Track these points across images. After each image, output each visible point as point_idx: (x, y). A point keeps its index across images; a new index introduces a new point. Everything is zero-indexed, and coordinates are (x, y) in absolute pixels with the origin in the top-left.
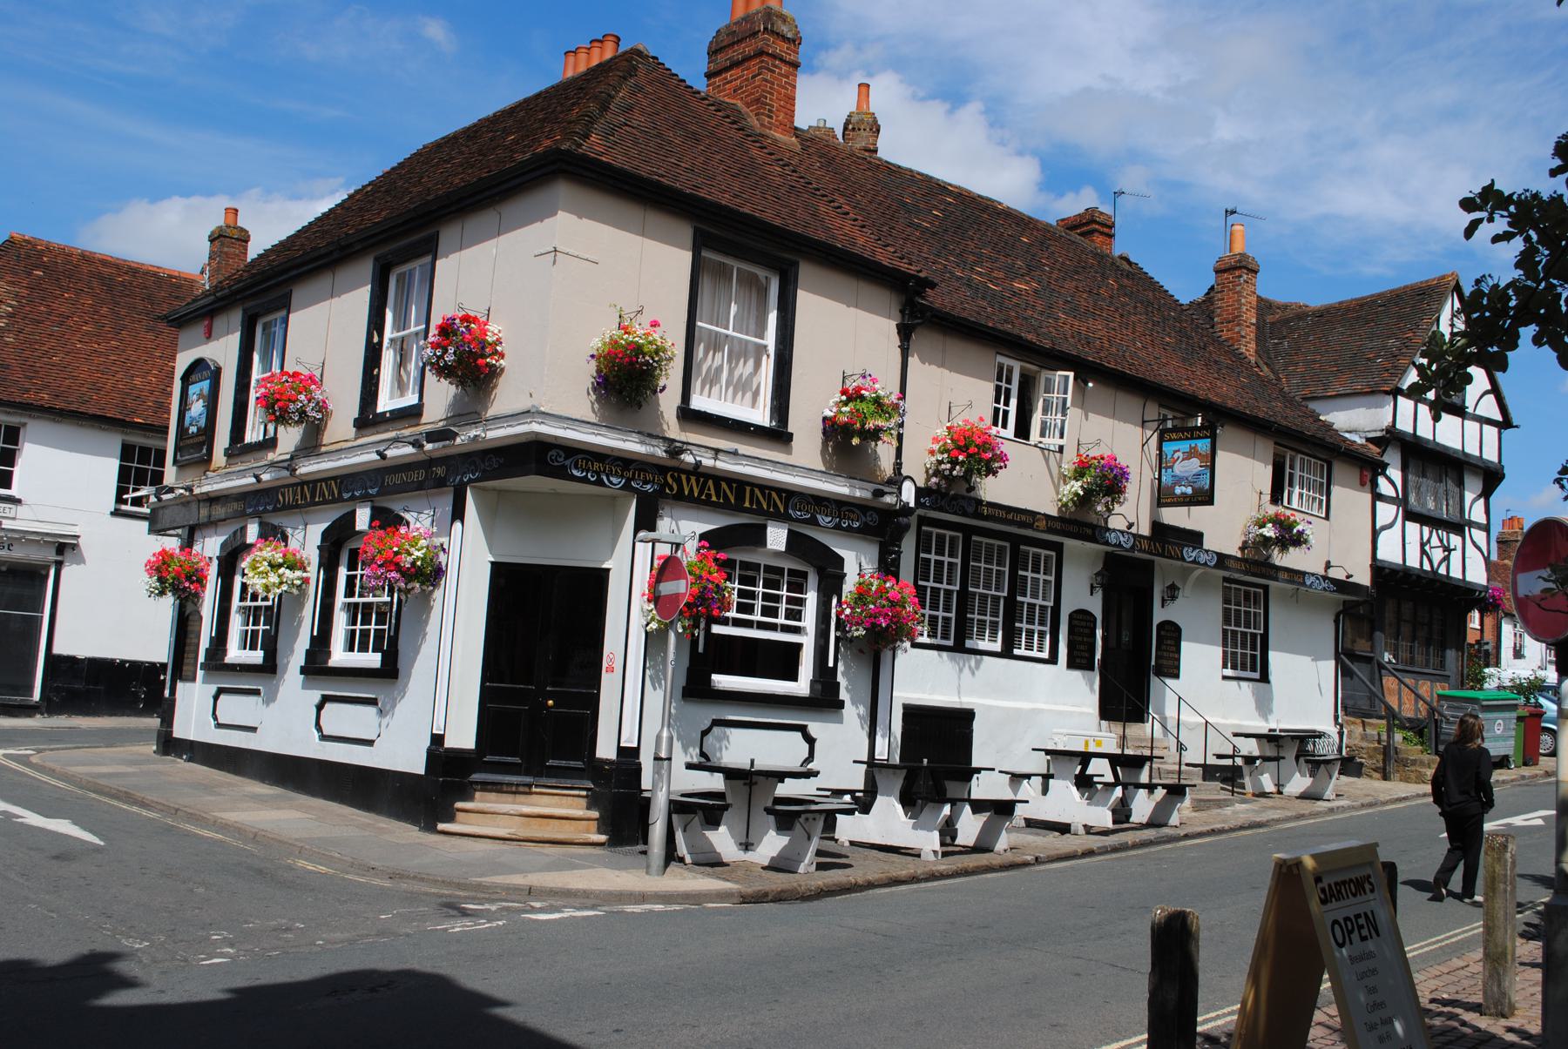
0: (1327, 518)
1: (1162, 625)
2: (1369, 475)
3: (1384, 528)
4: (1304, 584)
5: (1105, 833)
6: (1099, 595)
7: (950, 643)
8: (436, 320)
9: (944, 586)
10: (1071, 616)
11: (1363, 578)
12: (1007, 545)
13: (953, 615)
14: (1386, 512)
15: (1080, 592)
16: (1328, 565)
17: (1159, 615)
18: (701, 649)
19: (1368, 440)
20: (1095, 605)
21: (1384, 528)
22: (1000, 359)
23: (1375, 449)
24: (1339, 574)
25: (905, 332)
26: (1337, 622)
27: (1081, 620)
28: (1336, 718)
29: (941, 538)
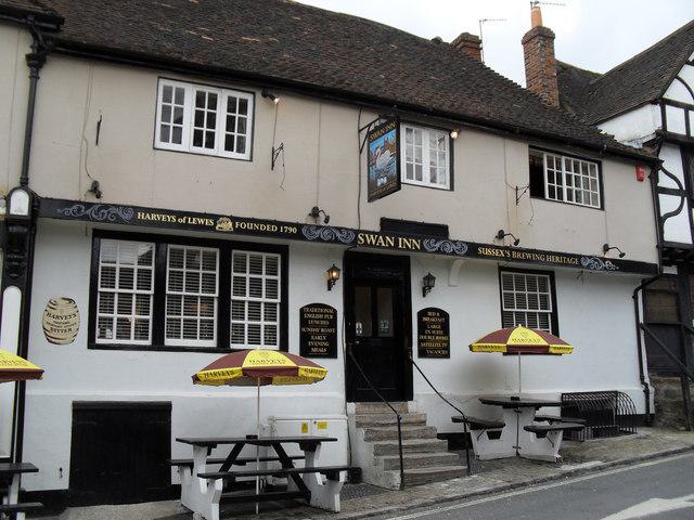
0: (602, 208)
1: (422, 314)
2: (646, 173)
3: (669, 215)
4: (580, 265)
5: (557, 420)
6: (339, 287)
7: (148, 343)
8: (556, 268)
9: (263, 299)
10: (302, 311)
11: (650, 256)
12: (217, 251)
13: (150, 317)
14: (669, 203)
15: (313, 286)
16: (606, 248)
17: (418, 304)
18: (641, 320)
19: (644, 144)
20: (336, 300)
21: (669, 215)
22: (163, 83)
23: (649, 151)
24: (613, 254)
25: (36, 62)
26: (635, 297)
27: (316, 317)
28: (642, 378)
29: (192, 255)
